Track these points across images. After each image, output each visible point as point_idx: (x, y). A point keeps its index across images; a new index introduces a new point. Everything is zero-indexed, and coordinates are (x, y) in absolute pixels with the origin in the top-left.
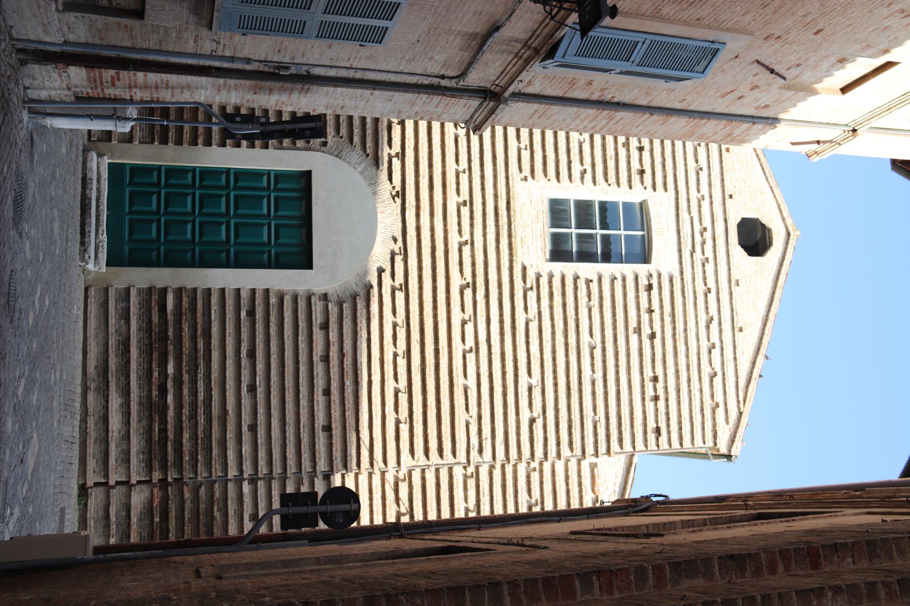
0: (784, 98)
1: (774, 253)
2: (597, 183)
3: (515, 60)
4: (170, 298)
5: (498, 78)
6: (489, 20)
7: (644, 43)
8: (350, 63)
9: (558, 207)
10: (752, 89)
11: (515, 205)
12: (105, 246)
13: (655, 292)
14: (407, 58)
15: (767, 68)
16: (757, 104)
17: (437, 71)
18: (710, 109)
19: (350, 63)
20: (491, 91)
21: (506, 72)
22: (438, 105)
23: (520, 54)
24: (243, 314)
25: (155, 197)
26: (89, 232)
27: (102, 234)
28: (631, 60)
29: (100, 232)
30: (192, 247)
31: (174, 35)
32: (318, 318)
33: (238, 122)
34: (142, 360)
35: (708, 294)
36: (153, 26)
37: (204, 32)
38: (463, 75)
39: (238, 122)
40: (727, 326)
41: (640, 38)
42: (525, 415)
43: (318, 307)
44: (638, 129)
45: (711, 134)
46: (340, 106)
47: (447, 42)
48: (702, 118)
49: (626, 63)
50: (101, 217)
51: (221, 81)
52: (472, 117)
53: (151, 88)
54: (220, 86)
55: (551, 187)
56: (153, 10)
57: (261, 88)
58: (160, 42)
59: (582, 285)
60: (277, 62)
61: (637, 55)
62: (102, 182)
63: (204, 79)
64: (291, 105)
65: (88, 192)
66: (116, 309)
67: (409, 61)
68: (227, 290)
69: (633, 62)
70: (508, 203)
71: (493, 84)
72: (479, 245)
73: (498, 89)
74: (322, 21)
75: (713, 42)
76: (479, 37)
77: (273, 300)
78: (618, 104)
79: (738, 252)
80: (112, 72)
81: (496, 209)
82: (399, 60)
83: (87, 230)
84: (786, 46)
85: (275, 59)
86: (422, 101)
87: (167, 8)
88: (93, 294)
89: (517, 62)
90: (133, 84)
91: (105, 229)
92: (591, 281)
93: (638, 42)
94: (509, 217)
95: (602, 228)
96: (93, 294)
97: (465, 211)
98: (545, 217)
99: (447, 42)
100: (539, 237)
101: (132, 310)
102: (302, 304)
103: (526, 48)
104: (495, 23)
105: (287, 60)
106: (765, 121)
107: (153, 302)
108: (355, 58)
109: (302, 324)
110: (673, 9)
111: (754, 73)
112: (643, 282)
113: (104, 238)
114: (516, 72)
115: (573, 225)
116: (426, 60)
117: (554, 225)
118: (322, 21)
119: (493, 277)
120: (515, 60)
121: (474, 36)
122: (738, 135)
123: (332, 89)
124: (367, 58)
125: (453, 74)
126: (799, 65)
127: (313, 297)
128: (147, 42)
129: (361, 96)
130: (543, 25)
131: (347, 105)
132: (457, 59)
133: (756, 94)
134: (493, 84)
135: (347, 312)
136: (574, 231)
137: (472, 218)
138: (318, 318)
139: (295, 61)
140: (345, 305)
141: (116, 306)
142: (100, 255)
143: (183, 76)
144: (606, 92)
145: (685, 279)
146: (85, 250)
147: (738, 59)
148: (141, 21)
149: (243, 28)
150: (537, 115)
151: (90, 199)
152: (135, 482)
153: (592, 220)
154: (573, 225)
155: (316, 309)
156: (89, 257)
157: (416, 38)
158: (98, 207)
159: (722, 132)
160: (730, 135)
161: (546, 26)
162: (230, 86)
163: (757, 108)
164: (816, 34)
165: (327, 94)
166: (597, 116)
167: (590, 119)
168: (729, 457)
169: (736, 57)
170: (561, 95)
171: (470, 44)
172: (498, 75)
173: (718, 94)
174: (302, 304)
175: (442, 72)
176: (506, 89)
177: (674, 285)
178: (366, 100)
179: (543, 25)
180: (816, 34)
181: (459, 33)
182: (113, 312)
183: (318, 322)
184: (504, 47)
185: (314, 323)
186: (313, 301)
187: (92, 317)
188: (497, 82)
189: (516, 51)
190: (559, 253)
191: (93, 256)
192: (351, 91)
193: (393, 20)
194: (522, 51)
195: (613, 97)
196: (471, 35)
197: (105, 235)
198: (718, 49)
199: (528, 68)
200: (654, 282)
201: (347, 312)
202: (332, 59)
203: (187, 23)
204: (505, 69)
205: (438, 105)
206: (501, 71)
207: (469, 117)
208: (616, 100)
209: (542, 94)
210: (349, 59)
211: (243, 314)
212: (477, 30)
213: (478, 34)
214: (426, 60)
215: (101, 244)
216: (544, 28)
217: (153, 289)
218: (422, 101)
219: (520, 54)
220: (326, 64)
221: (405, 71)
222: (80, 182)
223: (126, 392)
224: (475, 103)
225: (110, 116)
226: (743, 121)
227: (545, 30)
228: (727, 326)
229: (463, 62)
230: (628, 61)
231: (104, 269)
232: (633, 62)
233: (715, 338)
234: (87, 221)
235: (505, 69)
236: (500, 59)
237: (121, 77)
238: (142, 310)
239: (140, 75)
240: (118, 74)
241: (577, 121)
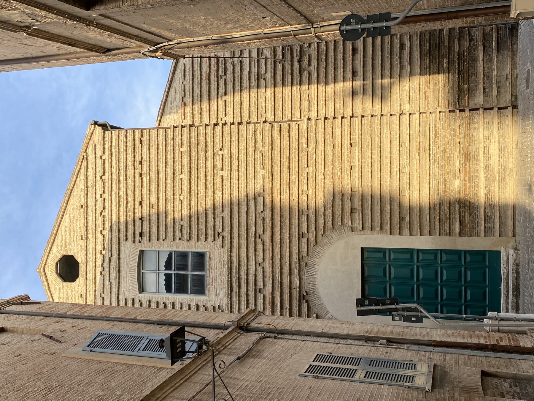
0: (43, 326)
1: (56, 254)
2: (172, 304)
3: (227, 344)
4: (457, 230)
5: (239, 336)
6: (244, 364)
7: (139, 350)
8: (338, 346)
9: (199, 288)
10: (65, 331)
11: (226, 288)
12: (502, 265)
13: (138, 232)
14: (299, 348)
15: (54, 340)
16: (62, 324)
17: (279, 341)
18: (95, 321)
19: (338, 346)
20: (244, 331)
21: (233, 339)
22: (279, 323)
23: (224, 347)
24: (408, 219)
25: (469, 298)
26: (513, 273)
27: (504, 273)
28: (148, 340)
29: (505, 274)
30: (442, 283)
31: (460, 362)
32: (358, 216)
33: (414, 316)
34: (476, 189)
35: (102, 229)
36: (475, 367)
37: (439, 363)
38: (261, 338)
39: (414, 316)
40: (91, 208)
41: (142, 353)
42: (226, 152)
43: (357, 223)
44: (145, 311)
45: (96, 308)
46: (344, 324)
47: (272, 354)
48: (101, 316)
49: (152, 338)
50: (505, 284)
51: (426, 338)
52: (256, 317)
53: (475, 336)
54: (427, 336)
55: (203, 301)
56: (475, 374)
57: (399, 334)
58: (469, 359)
59: (186, 236)
60: (388, 347)
61: (144, 343)
62: (505, 309)
63: (438, 339)
64: (377, 326)
65: (515, 301)
66: (494, 222)
67: (298, 346)
68: (419, 234)
69: (147, 338)
70: (231, 291)
71: (241, 334)
72: (252, 263)
73: (239, 331)
74: (358, 365)
75: (91, 351)
76: (251, 356)
77: (387, 227)
78: (158, 324)
79: (80, 258)
80: (501, 343)
81: (239, 287)
82: (305, 347)
83: (515, 275)
84: (41, 349)
85: (389, 349)
86: (289, 325)
87: (465, 376)
88: (510, 233)
89: (226, 343)
90: (487, 338)
91: (502, 276)
92: (180, 239)
93: (143, 350)
94: (231, 281)
95: (171, 274)
96: (510, 233)
97: (260, 285)
98: (208, 281)
99: (272, 354)
100: (213, 267)
101: (483, 222)
102: (368, 225)
103: (219, 350)
104: (240, 363)
105: (381, 349)
106: (57, 315)
107: (468, 226)
108: (335, 348)
109: (368, 211)
110: (118, 368)
111: (64, 337)
112: (145, 238)
113: (503, 270)
114: (227, 338)
115: (190, 269)
116: (286, 346)
117: (203, 277)
118: (358, 365)
119: (243, 242)
120: (227, 344)
121: (253, 357)
122: (77, 308)
123: (350, 333)
124: (326, 348)
125: (268, 339)
126: (33, 341)
127: (361, 229)
128: (478, 359)
129: (330, 329)
130: (207, 361)
131: (340, 325)
132: (266, 346)
133: (63, 328)
134: (241, 334)
135: (338, 219)
136: (189, 273)
137: (256, 281)
138: (358, 216)
139: (376, 348)
140: (340, 224)
141: (494, 224)
142: (505, 259)
143: (453, 341)
144: (166, 329)
145: (117, 239)
146: (515, 260)
147: (75, 344)
148: (483, 369)
149: (412, 364)
150: (213, 318)
151: (513, 295)
152: (481, 109)
153: (177, 280)
154: (190, 269)
155: (359, 221)
156: (513, 255)
157: (293, 357)
158: (508, 291)
159: (88, 309)
160: (82, 308)
161: (205, 360)
162: (420, 335)
163: (63, 322)
164: (20, 355)
165: (353, 330)
166: (173, 317)
167: (178, 315)
168: (96, 123)
169: (75, 345)
170: (196, 328)
171: (257, 353)
172: (238, 338)
173: (89, 328)
174: (368, 225)
175: (276, 340)
176: (233, 329)
177: (125, 236)
178: (327, 326)
179: (207, 361)
180: (20, 355)
181: (264, 358)
182: (496, 220)
183: (358, 213)
184: (234, 351)
185: (360, 212)
186: (361, 226)
187: (510, 216)
188: (239, 335)
189: (226, 349)
190: (200, 257)
191: (511, 257)
192: (337, 332)
193: (309, 365)
194: (222, 349)
195: (161, 327)
196: (256, 357)
197: (502, 272)
198: (88, 347)
199: (219, 339)
200: (138, 238)
201: (338, 219)
202: (350, 348)
203: (451, 368)
204: (234, 341)
205: (279, 323)
206: (236, 340)
207: (258, 317)
208: (160, 326)
209: (209, 329)
210: (339, 348)
211: (408, 219)
212: (252, 360)
213: (252, 358)
214: (286, 346)
215: (505, 266)
216: (207, 359)
217: (469, 235)
218: (289, 325)
219: (224, 347)
220: (354, 346)
221: (301, 341)
222: (520, 307)
223: (487, 167)
224: (253, 325)
225: (502, 320)
226: (73, 315)
227: (206, 358)
228: (91, 208)
229: (262, 345)
230: (150, 339)
231: (503, 250)
232: (147, 338)
233: (100, 201)
234: (515, 280)
235: (234, 341)
236: (237, 346)
237: (496, 341)
238: (476, 221)
239: (482, 341)
240: (498, 343)
241: (186, 315)
